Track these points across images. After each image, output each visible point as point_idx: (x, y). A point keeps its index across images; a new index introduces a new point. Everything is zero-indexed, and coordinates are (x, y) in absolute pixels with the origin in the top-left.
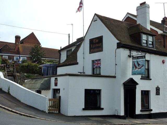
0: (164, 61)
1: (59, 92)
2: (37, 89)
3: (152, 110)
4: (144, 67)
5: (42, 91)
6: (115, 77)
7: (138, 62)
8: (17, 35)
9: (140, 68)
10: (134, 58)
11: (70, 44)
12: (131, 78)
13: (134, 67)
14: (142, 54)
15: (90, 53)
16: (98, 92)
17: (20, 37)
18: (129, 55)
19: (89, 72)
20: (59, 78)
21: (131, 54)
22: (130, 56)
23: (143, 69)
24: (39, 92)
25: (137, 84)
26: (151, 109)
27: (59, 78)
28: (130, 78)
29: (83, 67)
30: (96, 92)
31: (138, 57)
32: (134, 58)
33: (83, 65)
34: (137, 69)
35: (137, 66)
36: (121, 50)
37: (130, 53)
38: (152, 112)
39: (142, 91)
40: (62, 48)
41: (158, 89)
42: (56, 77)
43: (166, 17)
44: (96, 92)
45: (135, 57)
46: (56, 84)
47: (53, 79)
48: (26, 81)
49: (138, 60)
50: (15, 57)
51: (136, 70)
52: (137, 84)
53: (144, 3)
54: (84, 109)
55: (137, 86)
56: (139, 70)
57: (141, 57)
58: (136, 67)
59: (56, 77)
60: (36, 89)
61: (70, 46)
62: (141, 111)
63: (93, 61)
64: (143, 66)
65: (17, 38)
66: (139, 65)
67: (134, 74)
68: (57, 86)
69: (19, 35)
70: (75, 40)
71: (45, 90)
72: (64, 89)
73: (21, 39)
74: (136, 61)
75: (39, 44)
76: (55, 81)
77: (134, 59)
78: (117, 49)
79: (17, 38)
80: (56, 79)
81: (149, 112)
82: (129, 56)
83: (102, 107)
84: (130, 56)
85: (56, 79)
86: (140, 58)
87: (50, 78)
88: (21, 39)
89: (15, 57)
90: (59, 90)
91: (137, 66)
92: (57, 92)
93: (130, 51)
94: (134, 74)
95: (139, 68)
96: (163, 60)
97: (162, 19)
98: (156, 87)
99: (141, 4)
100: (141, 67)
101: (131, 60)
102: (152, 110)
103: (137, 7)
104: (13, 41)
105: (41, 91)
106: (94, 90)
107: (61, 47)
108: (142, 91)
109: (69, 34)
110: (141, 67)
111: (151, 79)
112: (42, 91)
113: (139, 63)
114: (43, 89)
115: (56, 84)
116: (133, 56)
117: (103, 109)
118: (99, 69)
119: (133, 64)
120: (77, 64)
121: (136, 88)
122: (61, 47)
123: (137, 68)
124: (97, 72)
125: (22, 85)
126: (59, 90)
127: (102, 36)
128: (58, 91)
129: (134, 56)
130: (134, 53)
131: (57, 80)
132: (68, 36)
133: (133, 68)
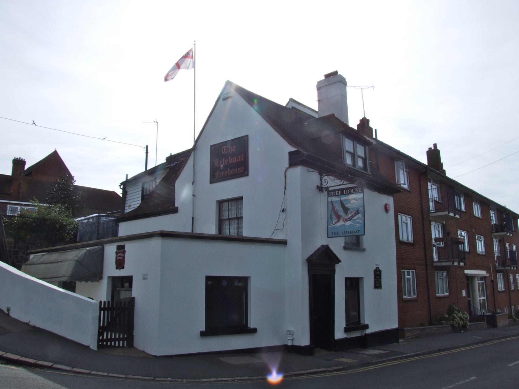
0: (388, 206)
1: (131, 286)
2: (64, 279)
3: (366, 327)
4: (360, 215)
5: (79, 285)
6: (284, 243)
7: (344, 203)
8: (18, 156)
9: (350, 219)
10: (330, 193)
11: (149, 168)
12: (324, 245)
13: (334, 216)
14: (342, 185)
15: (211, 182)
16: (240, 284)
17: (25, 162)
18: (319, 185)
19: (212, 230)
20: (129, 246)
21: (324, 183)
22: (320, 189)
23: (357, 221)
24: (69, 285)
25: (339, 261)
26: (366, 322)
27: (129, 246)
28: (322, 246)
29: (193, 218)
30: (236, 284)
31: (342, 190)
32: (330, 193)
33: (193, 214)
34: (341, 223)
35: (341, 213)
36: (298, 170)
37: (321, 180)
38: (368, 331)
39: (347, 279)
40: (129, 178)
41: (378, 273)
42: (119, 244)
43: (366, 118)
44: (236, 284)
45: (334, 190)
46: (120, 264)
47: (110, 250)
48: (31, 256)
49: (343, 198)
50: (8, 206)
51: (338, 224)
52: (339, 261)
53: (336, 73)
54: (203, 334)
55: (338, 267)
56: (348, 223)
57: (352, 191)
58: (339, 217)
59: (119, 244)
60: (59, 279)
61: (150, 173)
62: (346, 330)
63: (220, 203)
64: (358, 212)
65: (18, 163)
66: (346, 210)
67: (332, 234)
68: (123, 268)
69: (23, 157)
70: (162, 160)
71: (87, 281)
72: (145, 277)
73: (27, 167)
74: (336, 201)
75: (71, 178)
76: (117, 253)
77: (331, 196)
78: (288, 168)
79: (18, 163)
80: (121, 249)
81: (361, 331)
82: (318, 187)
83: (252, 325)
84: (320, 189)
85: (121, 249)
86: (347, 191)
87: (102, 244)
88: (27, 167)
89: (8, 206)
90: (129, 279)
91: (341, 213)
92: (123, 286)
93: (321, 174)
94: (332, 234)
95: (346, 217)
96: (386, 205)
97: (358, 123)
98: (375, 268)
99: (327, 76)
100: (352, 217)
101: (323, 198)
102: (366, 327)
103: (319, 83)
104: (8, 171)
105: (75, 283)
106: (132, 286)
107: (127, 175)
108: (347, 279)
109: (147, 147)
110: (352, 217)
111: (364, 250)
112: (79, 285)
113: (348, 206)
114: (81, 279)
115: (120, 264)
116: (327, 189)
117: (254, 331)
118: (238, 224)
119: (330, 209)
120: (175, 210)
121: (334, 272)
122: (127, 175)
123: (342, 219)
124: (231, 230)
125: (19, 268)
126: (129, 279)
127: (247, 136)
128: (127, 285)
129: (330, 189)
130: (331, 182)
131: (124, 252)
132: (145, 151)
133: (331, 218)
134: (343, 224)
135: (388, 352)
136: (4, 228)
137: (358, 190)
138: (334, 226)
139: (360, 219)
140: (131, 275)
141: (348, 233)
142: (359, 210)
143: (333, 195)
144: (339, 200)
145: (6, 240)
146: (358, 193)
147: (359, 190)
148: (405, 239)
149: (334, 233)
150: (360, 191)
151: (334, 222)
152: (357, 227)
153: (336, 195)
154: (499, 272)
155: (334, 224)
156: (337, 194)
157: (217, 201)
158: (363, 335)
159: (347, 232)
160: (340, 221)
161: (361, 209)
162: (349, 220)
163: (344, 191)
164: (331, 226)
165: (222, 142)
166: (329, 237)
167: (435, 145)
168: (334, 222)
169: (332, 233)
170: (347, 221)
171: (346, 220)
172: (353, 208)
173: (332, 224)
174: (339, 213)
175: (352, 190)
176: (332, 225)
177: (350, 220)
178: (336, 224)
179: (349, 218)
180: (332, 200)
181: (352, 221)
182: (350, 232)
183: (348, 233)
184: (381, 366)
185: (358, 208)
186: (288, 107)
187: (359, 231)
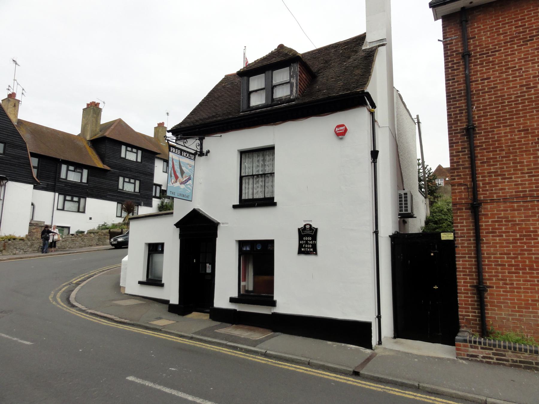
34: (178, 184)
35: (179, 174)
56: (183, 186)
108: (241, 244)
136: (528, 111)
138: (172, 185)
139: (190, 186)
140: (35, 190)
145: (520, 264)
148: (306, 226)
151: (173, 181)
155: (172, 184)
157: (274, 145)
167: (416, 217)
168: (173, 181)
171: (181, 183)
176: (171, 183)
177: (184, 184)
178: (174, 184)
179: (184, 182)
181: (185, 186)
184: (109, 325)
186: (270, 72)
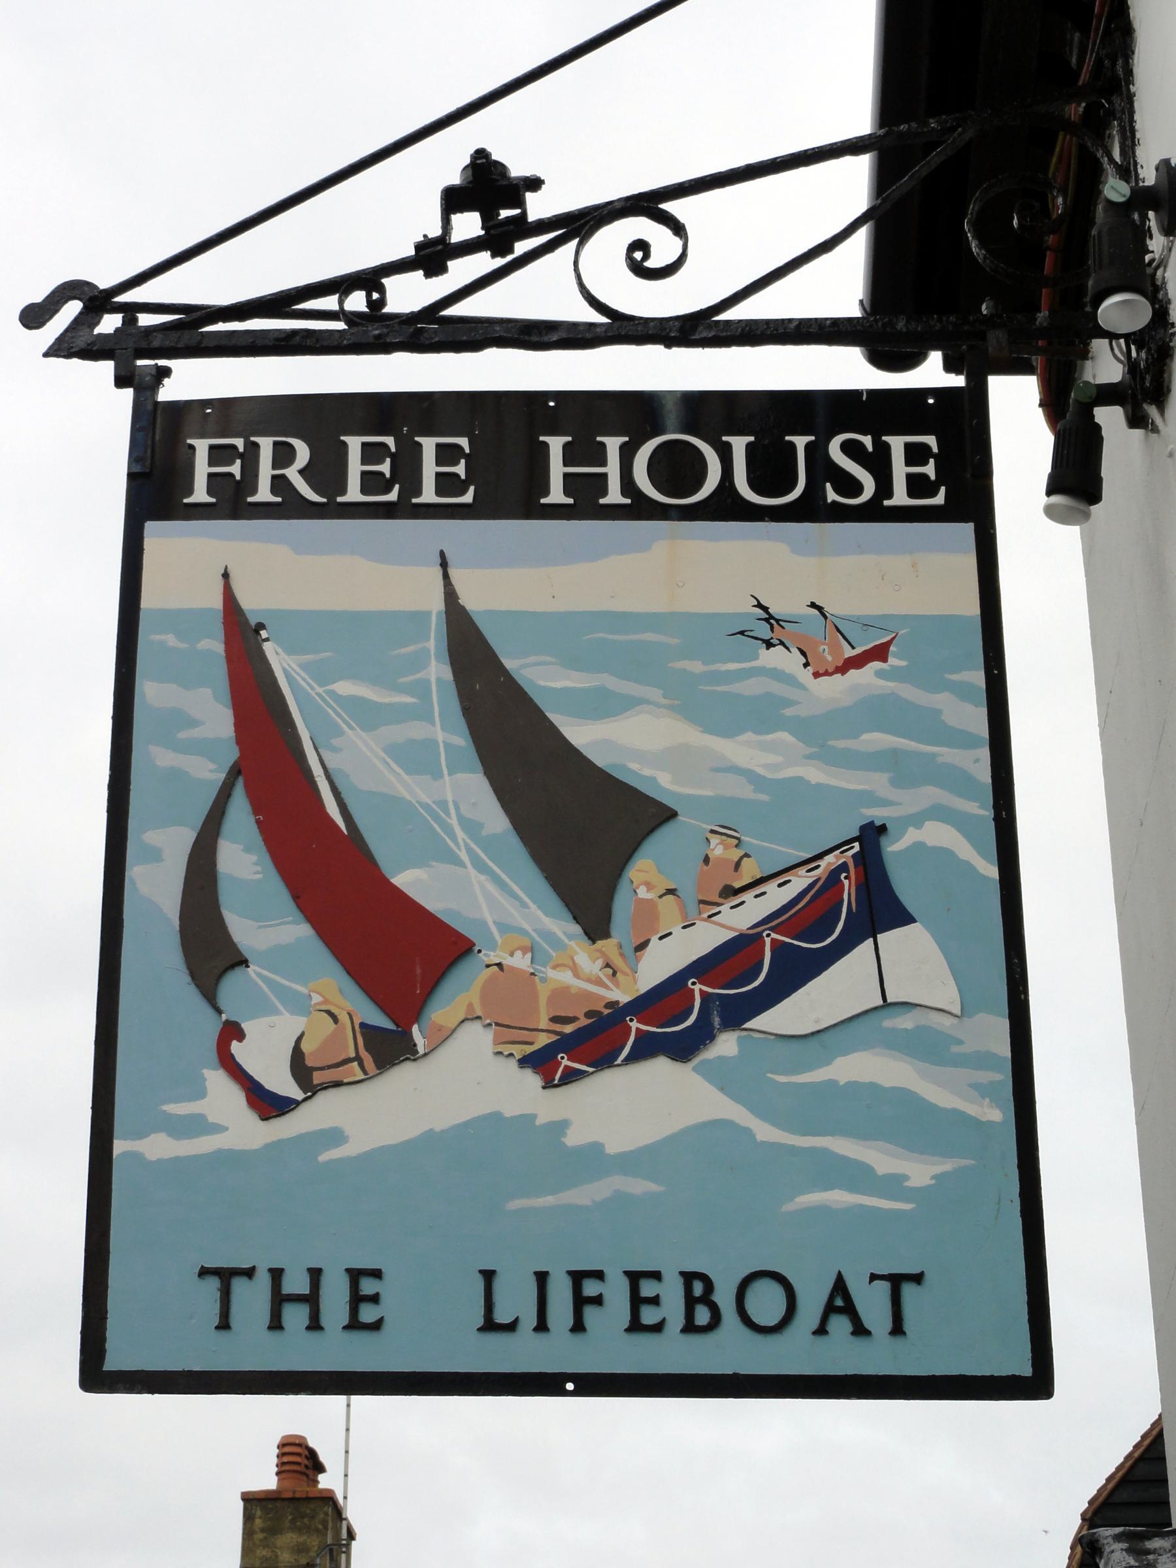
6: (224, 1324)
134: (495, 1119)
135: (841, 744)
137: (879, 464)
141: (636, 1326)
142: (893, 848)
143: (264, 494)
144: (436, 603)
146: (875, 512)
147: (900, 470)
149: (279, 1299)
150: (917, 485)
152: (839, 1197)
153: (354, 493)
154: (353, 1058)
156: (370, 482)
158: (937, 117)
159: (616, 1292)
160: (442, 1037)
161: (938, 834)
162: (645, 1049)
163: (556, 444)
164: (198, 1126)
165: (563, 1014)
166: (113, 1362)
169: (226, 1276)
170: (604, 1061)
172: (746, 792)
173: (218, 1081)
174: (405, 880)
175: (739, 444)
180: (250, 602)
182: (672, 1294)
183: (636, 1326)
185: (878, 814)
187: (896, 1281)
